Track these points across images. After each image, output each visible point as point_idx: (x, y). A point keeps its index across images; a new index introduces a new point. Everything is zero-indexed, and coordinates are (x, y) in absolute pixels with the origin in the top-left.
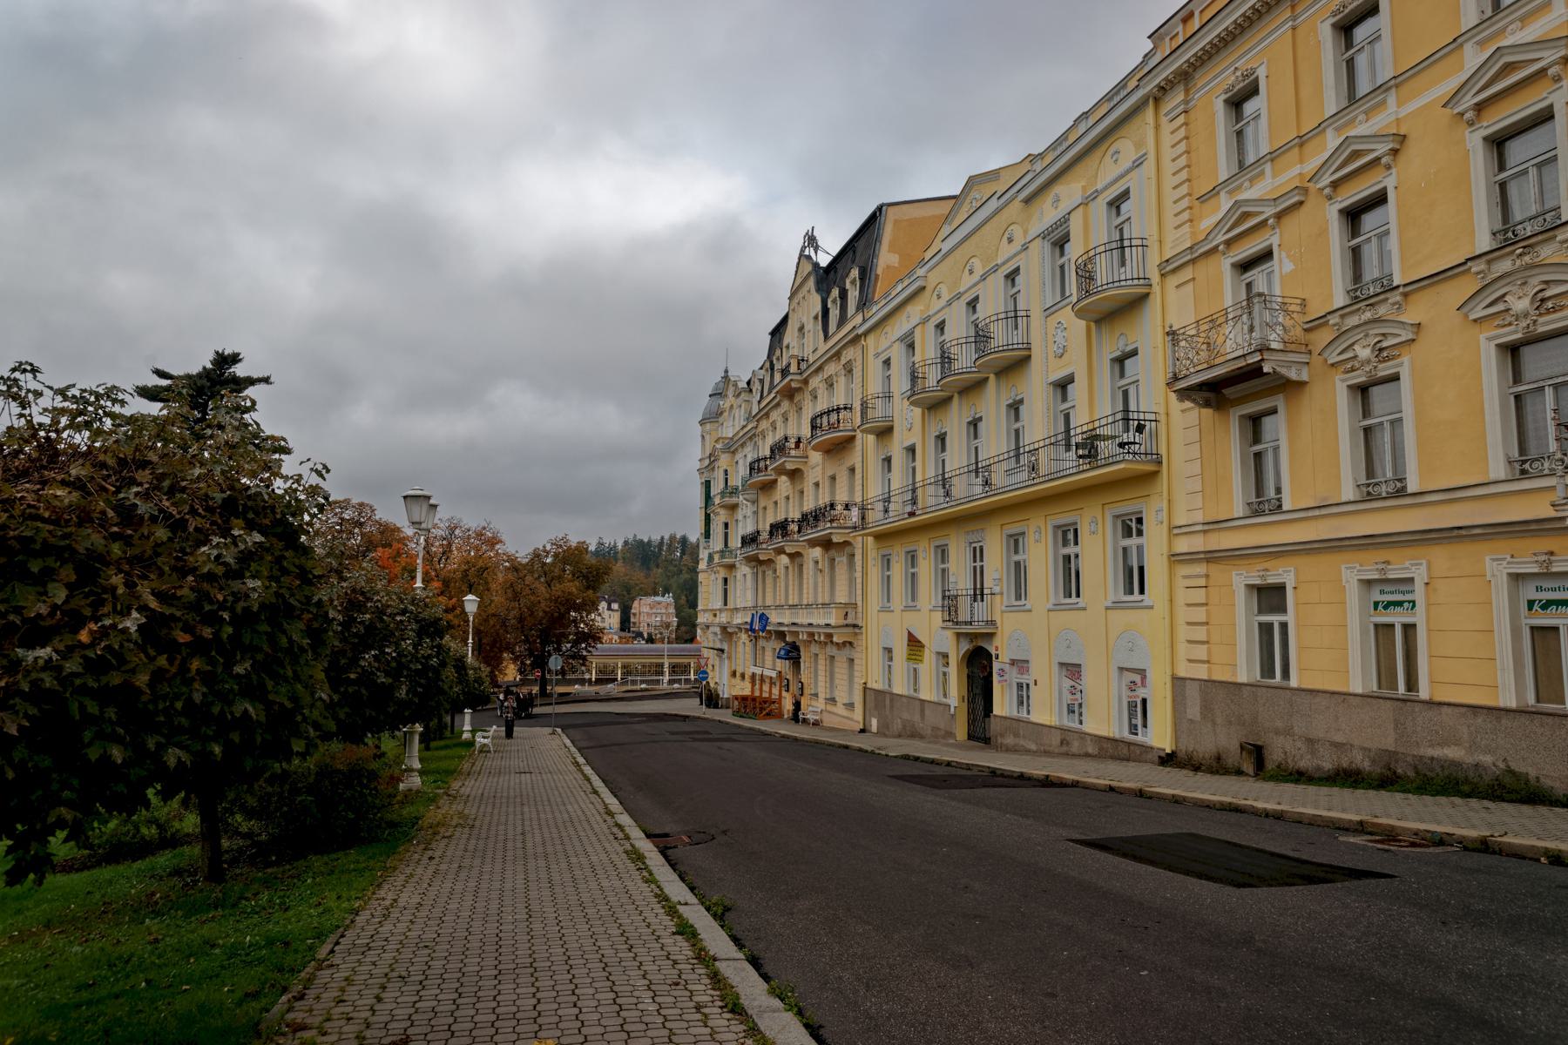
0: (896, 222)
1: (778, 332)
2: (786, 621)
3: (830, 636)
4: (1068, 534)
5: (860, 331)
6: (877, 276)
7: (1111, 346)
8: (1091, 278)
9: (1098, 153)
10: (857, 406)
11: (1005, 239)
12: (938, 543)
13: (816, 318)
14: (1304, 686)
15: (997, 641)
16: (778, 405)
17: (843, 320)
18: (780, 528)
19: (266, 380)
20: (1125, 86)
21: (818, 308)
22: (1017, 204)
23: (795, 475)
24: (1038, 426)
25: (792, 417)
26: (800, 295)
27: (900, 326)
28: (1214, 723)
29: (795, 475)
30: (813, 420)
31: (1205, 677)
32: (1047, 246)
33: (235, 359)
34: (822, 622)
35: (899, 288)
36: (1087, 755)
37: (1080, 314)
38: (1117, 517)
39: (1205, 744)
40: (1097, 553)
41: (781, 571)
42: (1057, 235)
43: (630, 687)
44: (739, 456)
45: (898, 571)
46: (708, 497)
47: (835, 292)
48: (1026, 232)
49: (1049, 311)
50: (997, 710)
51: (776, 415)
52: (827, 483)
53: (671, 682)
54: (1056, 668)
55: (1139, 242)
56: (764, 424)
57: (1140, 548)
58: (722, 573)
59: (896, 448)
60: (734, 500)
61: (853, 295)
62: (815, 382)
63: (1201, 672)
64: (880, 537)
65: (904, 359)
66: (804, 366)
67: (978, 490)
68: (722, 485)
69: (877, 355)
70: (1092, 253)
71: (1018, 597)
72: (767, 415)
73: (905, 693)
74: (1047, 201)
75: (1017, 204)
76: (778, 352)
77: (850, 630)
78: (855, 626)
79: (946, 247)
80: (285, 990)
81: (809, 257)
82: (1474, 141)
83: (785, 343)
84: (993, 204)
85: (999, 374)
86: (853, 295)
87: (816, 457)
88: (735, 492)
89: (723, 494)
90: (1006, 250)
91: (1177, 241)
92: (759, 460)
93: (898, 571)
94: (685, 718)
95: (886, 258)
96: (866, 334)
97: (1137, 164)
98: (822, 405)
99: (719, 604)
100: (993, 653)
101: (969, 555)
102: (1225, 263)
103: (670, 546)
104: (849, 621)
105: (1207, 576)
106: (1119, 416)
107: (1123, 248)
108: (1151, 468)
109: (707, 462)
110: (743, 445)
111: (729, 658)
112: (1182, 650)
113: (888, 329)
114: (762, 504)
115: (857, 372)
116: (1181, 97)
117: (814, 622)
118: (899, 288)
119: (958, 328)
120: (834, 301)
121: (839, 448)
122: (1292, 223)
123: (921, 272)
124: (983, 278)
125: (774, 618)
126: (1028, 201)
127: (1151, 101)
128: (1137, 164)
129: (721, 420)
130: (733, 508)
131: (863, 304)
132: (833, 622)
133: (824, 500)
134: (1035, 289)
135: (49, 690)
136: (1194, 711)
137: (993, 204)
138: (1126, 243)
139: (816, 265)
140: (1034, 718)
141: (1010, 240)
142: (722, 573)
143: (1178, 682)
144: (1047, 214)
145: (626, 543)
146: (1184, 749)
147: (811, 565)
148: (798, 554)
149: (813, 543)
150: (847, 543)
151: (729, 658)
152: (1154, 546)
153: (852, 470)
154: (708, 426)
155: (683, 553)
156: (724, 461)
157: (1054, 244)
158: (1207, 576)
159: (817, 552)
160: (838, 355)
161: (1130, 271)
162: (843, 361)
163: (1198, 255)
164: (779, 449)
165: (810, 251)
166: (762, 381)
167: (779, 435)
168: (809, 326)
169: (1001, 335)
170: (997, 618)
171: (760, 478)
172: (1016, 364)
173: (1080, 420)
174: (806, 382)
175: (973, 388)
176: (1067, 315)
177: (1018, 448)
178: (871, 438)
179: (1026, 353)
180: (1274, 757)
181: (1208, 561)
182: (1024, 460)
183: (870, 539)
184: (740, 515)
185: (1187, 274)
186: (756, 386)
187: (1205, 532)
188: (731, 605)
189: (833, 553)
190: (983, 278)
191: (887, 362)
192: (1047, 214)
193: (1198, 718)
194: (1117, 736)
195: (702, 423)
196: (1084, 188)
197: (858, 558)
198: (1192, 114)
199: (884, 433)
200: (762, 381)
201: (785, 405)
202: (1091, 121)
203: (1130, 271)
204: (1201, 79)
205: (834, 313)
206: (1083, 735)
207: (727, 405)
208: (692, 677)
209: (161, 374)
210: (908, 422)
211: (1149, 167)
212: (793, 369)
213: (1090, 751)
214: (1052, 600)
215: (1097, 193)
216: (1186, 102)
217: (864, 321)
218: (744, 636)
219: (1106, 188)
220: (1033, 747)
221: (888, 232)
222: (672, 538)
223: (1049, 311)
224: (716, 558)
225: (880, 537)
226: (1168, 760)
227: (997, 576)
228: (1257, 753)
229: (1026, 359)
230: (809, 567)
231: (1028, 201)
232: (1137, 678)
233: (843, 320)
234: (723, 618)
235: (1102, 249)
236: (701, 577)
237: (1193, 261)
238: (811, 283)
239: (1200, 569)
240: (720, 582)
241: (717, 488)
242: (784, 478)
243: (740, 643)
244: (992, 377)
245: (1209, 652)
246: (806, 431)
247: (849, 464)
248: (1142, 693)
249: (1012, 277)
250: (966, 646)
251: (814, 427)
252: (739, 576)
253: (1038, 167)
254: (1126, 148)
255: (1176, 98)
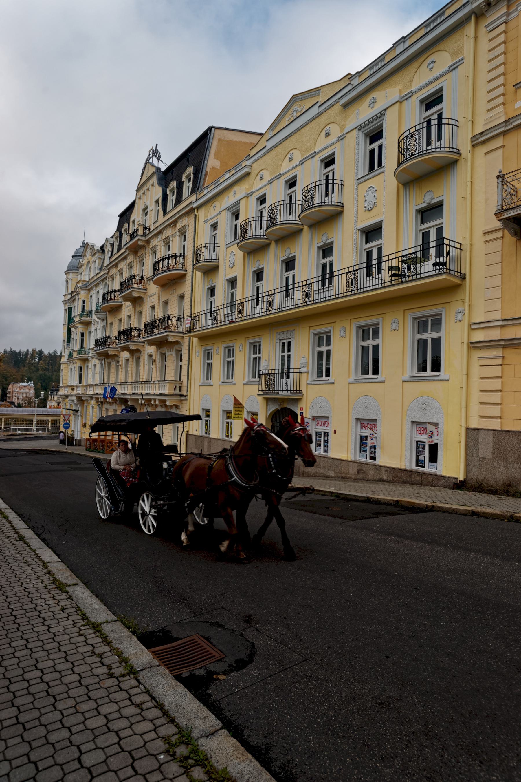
0: (220, 140)
1: (125, 216)
2: (128, 392)
3: (165, 401)
4: (323, 339)
5: (194, 206)
6: (206, 172)
8: (246, 232)
9: (416, 64)
10: (189, 254)
11: (323, 134)
12: (252, 341)
13: (157, 202)
14: (504, 429)
15: (302, 404)
16: (125, 258)
17: (179, 200)
18: (126, 334)
20: (383, 59)
22: (337, 108)
23: (137, 301)
26: (145, 188)
27: (229, 200)
28: (506, 460)
29: (137, 301)
30: (104, 295)
31: (498, 428)
32: (362, 136)
34: (158, 392)
35: (228, 175)
36: (382, 481)
37: (241, 248)
38: (226, 347)
39: (498, 474)
40: (397, 344)
41: (122, 362)
42: (234, 209)
43: (11, 433)
44: (93, 292)
45: (218, 362)
46: (70, 319)
48: (342, 128)
49: (228, 246)
51: (122, 265)
52: (161, 306)
53: (38, 430)
54: (221, 412)
55: (339, 182)
56: (113, 271)
57: (376, 348)
58: (79, 364)
59: (220, 283)
60: (89, 319)
61: (188, 185)
62: (154, 242)
63: (495, 425)
64: (204, 338)
65: (229, 223)
66: (147, 231)
67: (211, 322)
68: (80, 310)
69: (206, 221)
70: (247, 221)
71: (207, 379)
72: (116, 265)
73: (220, 437)
75: (337, 108)
76: (126, 226)
77: (178, 397)
78: (181, 395)
79: (270, 145)
83: (132, 219)
84: (315, 110)
85: (277, 241)
86: (188, 185)
87: (153, 288)
88: (90, 313)
89: (81, 315)
90: (286, 166)
92: (108, 293)
93: (218, 362)
94: (54, 452)
95: (212, 162)
96: (198, 208)
97: (453, 68)
98: (161, 254)
99: (76, 383)
100: (298, 412)
101: (279, 348)
104: (177, 392)
105: (503, 357)
106: (209, 311)
107: (261, 220)
108: (458, 281)
109: (69, 297)
110: (96, 285)
111: (82, 416)
112: (475, 410)
113: (217, 204)
114: (109, 321)
115: (190, 234)
116: (504, 10)
117: (151, 392)
118: (228, 175)
120: (172, 191)
121: (171, 282)
123: (249, 163)
124: (270, 182)
125: (120, 390)
126: (346, 106)
127: (473, 18)
128: (453, 68)
129: (80, 271)
130: (88, 324)
131: (195, 189)
132: (166, 392)
133: (159, 314)
137: (315, 110)
138: (293, 202)
139: (158, 169)
140: (332, 454)
141: (261, 179)
142: (79, 364)
144: (364, 112)
146: (474, 478)
147: (147, 357)
148: (138, 351)
149: (151, 343)
150: (177, 343)
151: (82, 416)
152: (454, 339)
153: (182, 297)
154: (71, 275)
156: (82, 295)
157: (233, 214)
158: (503, 357)
159: (151, 349)
160: (175, 223)
161: (332, 198)
162: (119, 268)
164: (126, 284)
165: (155, 161)
166: (112, 245)
167: (126, 275)
168: (152, 206)
170: (303, 389)
172: (333, 216)
173: (238, 297)
174: (148, 242)
175: (291, 235)
176: (235, 249)
177: (232, 302)
178: (199, 275)
179: (217, 264)
181: (504, 347)
182: (236, 309)
183: (195, 340)
184: (92, 328)
185: (499, 142)
186: (108, 248)
187: (502, 326)
188: (84, 383)
189: (164, 349)
190: (270, 182)
191: (214, 227)
192: (364, 112)
193: (490, 456)
194: (408, 468)
196: (400, 91)
197: (185, 353)
198: (512, 25)
199: (211, 270)
200: (112, 245)
201: (131, 258)
202: (407, 44)
203: (332, 198)
205: (172, 198)
206: (379, 468)
208: (50, 427)
210: (232, 261)
211: (466, 69)
212: (140, 232)
213: (385, 477)
214: (222, 380)
215: (253, 193)
216: (508, 14)
217: (197, 200)
218: (93, 402)
219: (321, 151)
220: (332, 474)
221: (214, 146)
223: (228, 246)
224: (75, 355)
225: (204, 338)
226: (460, 486)
227: (304, 360)
229: (340, 213)
230: (144, 359)
231: (346, 106)
232: (433, 428)
233: (179, 200)
234: (79, 391)
235: (282, 203)
236: (62, 367)
237: (504, 133)
238: (155, 179)
239: (499, 352)
240: (77, 369)
241: (77, 311)
242: (128, 303)
243: (90, 407)
244: (306, 227)
245: (502, 411)
246: (148, 272)
247: (180, 292)
249: (329, 162)
250: (273, 408)
251: (155, 269)
252: (90, 365)
253: (355, 82)
254: (442, 59)
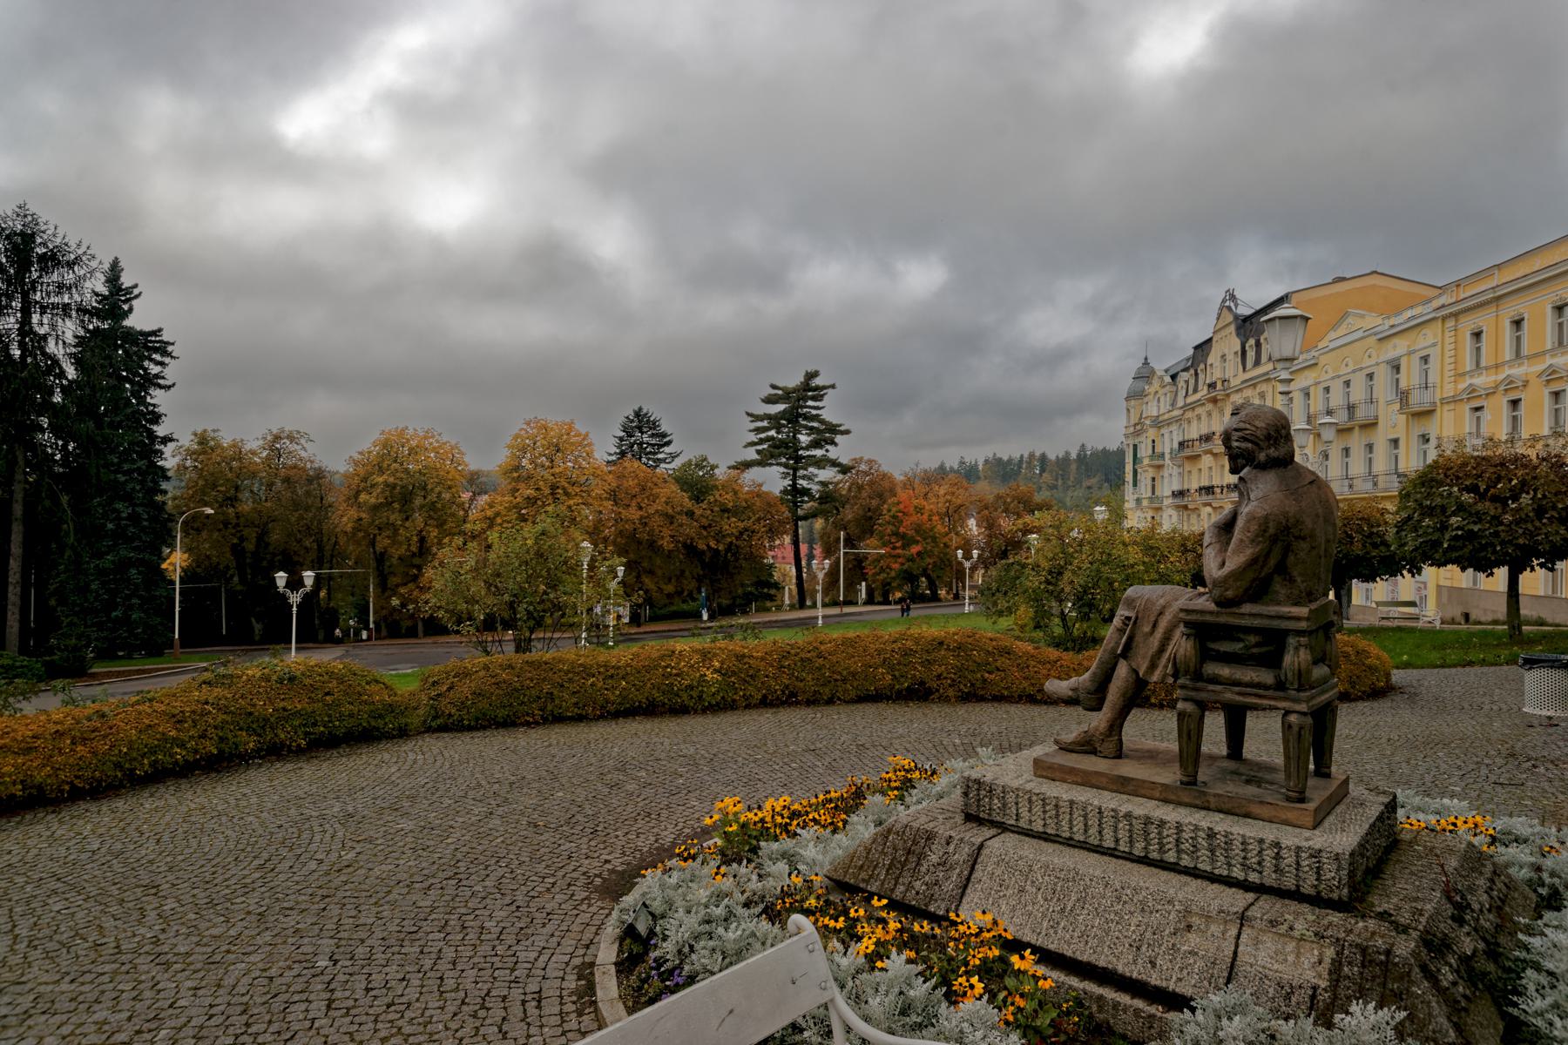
7: (1417, 430)
19: (833, 387)
21: (1238, 348)
24: (1381, 465)
25: (1215, 414)
33: (815, 374)
47: (1252, 342)
50: (1354, 601)
63: (1448, 583)
74: (1390, 344)
79: (1332, 345)
80: (985, 680)
81: (1229, 308)
82: (1546, 392)
91: (1449, 391)
102: (1467, 407)
103: (1029, 463)
119: (1337, 399)
122: (1492, 399)
134: (1383, 388)
135: (161, 574)
136: (1445, 599)
137: (1360, 334)
143: (1439, 587)
145: (986, 461)
155: (1043, 470)
163: (1454, 400)
169: (1361, 414)
171: (1188, 452)
172: (1370, 425)
180: (1473, 617)
184: (1166, 473)
195: (1127, 399)
204: (1463, 319)
205: (1251, 354)
207: (1152, 390)
209: (774, 387)
222: (1032, 455)
223: (1389, 403)
228: (1467, 616)
248: (1424, 593)
255: (1451, 323)
